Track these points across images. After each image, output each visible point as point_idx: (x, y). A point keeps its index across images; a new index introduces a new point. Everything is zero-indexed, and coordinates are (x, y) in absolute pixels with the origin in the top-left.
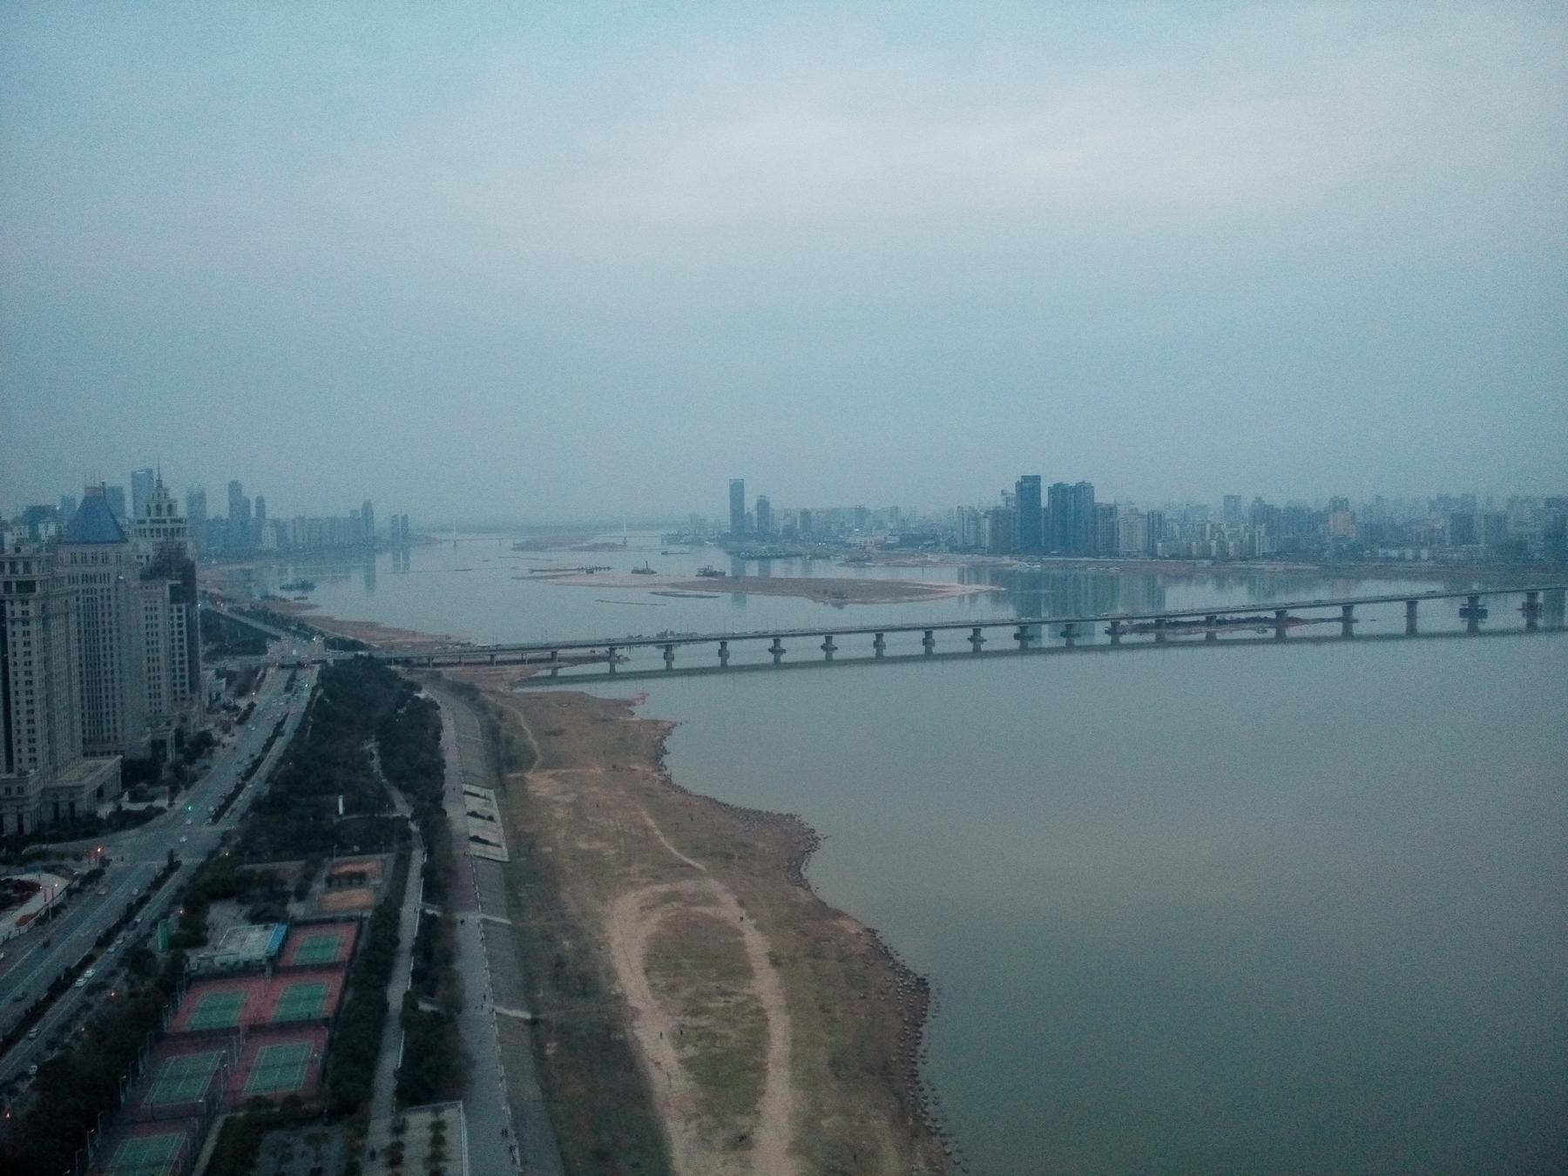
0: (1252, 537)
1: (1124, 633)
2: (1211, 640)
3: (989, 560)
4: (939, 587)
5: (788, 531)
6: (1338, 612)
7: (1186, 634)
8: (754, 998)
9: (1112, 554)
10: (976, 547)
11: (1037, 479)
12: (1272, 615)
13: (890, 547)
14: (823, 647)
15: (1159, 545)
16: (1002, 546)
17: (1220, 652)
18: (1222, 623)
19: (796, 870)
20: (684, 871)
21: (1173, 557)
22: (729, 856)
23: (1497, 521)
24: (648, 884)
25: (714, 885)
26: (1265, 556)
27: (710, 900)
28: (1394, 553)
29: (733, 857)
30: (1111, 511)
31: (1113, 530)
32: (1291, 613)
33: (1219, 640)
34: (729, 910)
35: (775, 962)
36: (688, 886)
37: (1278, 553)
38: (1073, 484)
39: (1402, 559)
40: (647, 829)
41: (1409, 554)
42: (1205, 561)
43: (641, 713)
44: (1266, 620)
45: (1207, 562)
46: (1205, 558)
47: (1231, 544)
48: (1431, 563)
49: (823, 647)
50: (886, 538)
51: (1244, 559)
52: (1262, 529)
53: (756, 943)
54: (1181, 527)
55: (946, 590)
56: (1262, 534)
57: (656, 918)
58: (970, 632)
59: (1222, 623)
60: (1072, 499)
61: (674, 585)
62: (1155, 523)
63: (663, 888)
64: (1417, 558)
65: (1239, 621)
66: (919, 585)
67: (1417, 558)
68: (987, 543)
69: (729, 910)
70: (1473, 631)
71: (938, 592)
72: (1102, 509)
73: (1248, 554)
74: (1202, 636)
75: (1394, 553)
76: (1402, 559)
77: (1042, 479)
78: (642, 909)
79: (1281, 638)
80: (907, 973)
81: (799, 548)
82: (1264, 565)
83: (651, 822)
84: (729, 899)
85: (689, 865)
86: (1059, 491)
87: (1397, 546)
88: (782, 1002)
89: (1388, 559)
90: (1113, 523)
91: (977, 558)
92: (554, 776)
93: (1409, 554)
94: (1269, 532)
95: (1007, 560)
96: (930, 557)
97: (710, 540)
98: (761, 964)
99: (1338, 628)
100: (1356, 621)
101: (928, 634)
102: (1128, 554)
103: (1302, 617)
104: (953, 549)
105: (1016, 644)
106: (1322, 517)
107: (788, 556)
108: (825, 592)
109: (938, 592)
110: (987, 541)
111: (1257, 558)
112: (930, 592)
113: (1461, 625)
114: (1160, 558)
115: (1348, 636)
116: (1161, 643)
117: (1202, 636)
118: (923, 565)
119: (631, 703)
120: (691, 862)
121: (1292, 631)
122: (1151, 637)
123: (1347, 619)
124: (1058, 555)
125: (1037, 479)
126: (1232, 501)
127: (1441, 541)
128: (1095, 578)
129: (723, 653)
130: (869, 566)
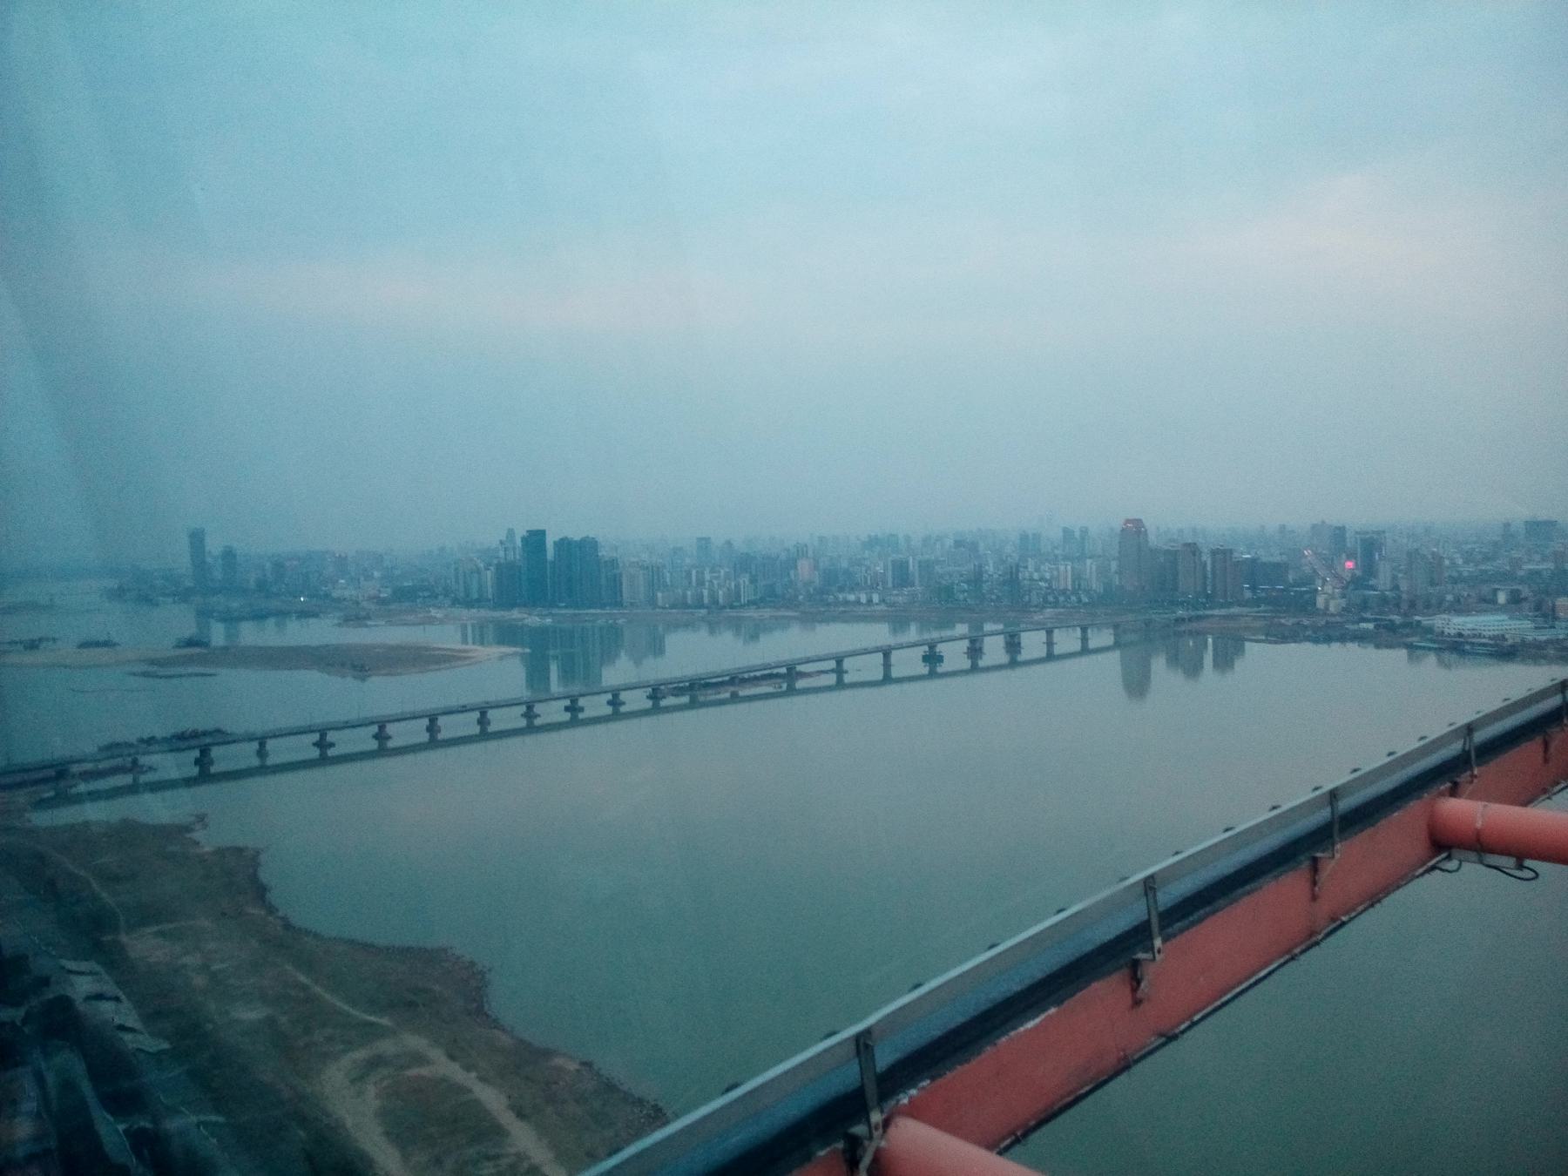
0: (737, 586)
1: (664, 697)
2: (735, 699)
3: (498, 614)
4: (460, 651)
5: (262, 586)
6: (832, 664)
7: (715, 694)
8: (520, 1157)
9: (619, 604)
10: (478, 600)
11: (543, 533)
12: (783, 670)
13: (383, 602)
14: (376, 737)
15: (659, 595)
16: (505, 599)
17: (742, 707)
18: (744, 681)
19: (480, 1011)
20: (371, 1033)
21: (673, 607)
22: (411, 1005)
23: (926, 567)
24: (345, 1051)
25: (415, 1042)
26: (751, 603)
27: (419, 1059)
28: (852, 597)
29: (417, 1005)
30: (613, 563)
31: (616, 582)
32: (800, 668)
33: (742, 697)
34: (443, 1067)
35: (521, 1115)
36: (386, 1047)
37: (762, 600)
38: (577, 538)
39: (858, 602)
40: (304, 988)
41: (864, 599)
42: (702, 611)
43: (208, 840)
44: (777, 676)
45: (704, 611)
46: (700, 608)
47: (720, 592)
48: (883, 607)
49: (376, 737)
50: (379, 591)
51: (732, 607)
52: (744, 580)
53: (492, 1098)
54: (671, 574)
55: (470, 655)
56: (747, 583)
57: (371, 1090)
58: (523, 709)
59: (744, 681)
60: (579, 552)
61: (152, 662)
62: (654, 575)
63: (360, 1054)
64: (870, 601)
65: (756, 678)
66: (439, 649)
67: (870, 601)
68: (490, 592)
69: (443, 1067)
70: (933, 674)
71: (465, 658)
72: (606, 562)
73: (734, 602)
74: (727, 695)
75: (852, 597)
76: (858, 602)
77: (547, 533)
78: (353, 1081)
79: (792, 691)
80: (640, 1102)
81: (275, 604)
82: (752, 613)
83: (302, 978)
84: (437, 1054)
85: (372, 1024)
86: (564, 544)
87: (852, 590)
88: (551, 1155)
89: (846, 603)
90: (615, 575)
91: (484, 613)
92: (162, 934)
93: (864, 599)
94: (753, 581)
95: (516, 614)
96: (433, 612)
97: (164, 595)
98: (507, 1119)
99: (831, 679)
100: (846, 672)
101: (483, 714)
102: (632, 604)
103: (807, 671)
104: (456, 602)
105: (567, 716)
106: (792, 563)
107: (260, 616)
108: (343, 665)
109: (465, 658)
110: (490, 590)
111: (742, 606)
112: (459, 658)
113: (924, 669)
114: (659, 608)
115: (840, 685)
116: (694, 704)
117: (727, 695)
118: (431, 621)
119: (187, 829)
120: (372, 1018)
121: (800, 684)
122: (685, 699)
123: (839, 671)
124: (566, 607)
125: (543, 533)
126: (704, 544)
127: (885, 583)
128: (601, 629)
129: (262, 753)
130: (371, 626)
